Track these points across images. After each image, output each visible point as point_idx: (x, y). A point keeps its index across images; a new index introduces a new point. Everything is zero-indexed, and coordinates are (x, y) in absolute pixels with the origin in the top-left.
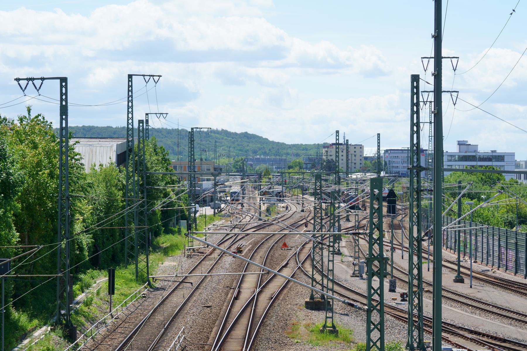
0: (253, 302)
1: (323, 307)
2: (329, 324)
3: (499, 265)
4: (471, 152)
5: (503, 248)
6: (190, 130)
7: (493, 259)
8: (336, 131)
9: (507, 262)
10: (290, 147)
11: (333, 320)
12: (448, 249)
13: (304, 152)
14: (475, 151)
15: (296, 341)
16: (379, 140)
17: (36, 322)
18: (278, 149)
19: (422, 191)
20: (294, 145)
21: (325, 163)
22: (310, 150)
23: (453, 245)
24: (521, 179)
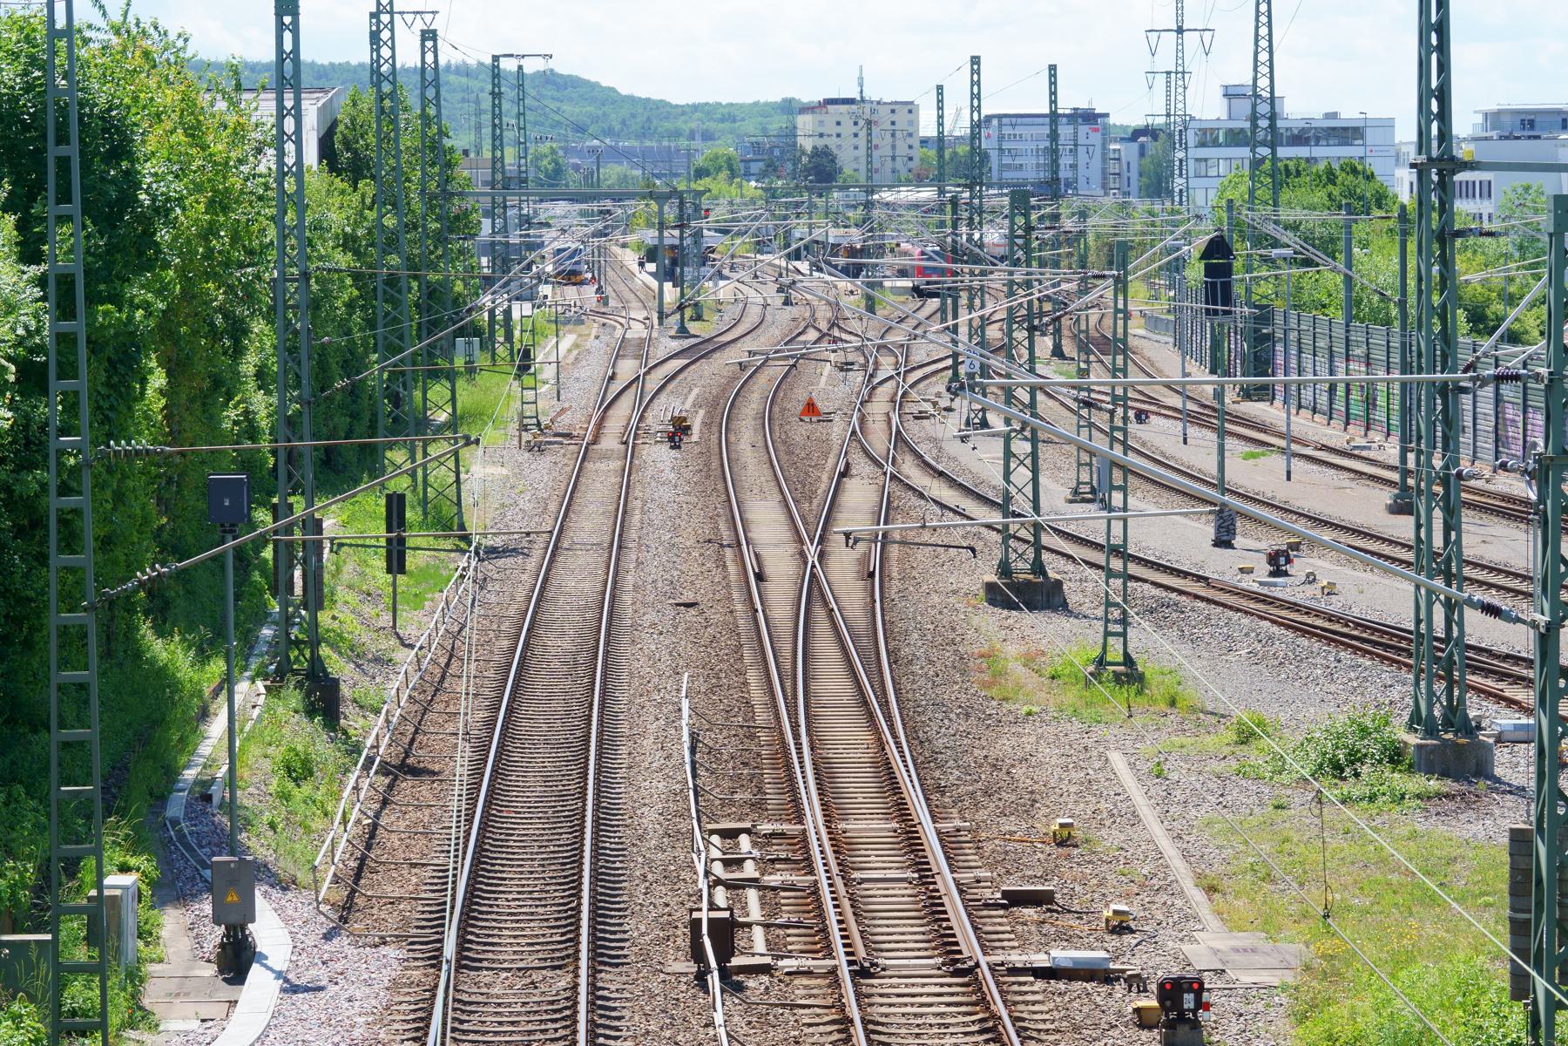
0: (813, 591)
5: (1510, 406)
6: (488, 61)
7: (1475, 441)
8: (972, 57)
10: (684, 113)
12: (1302, 411)
13: (726, 125)
15: (1025, 709)
16: (1055, 83)
17: (217, 667)
18: (649, 120)
19: (1460, 234)
20: (695, 108)
21: (805, 159)
22: (743, 120)
23: (1323, 399)
24: (1490, 196)
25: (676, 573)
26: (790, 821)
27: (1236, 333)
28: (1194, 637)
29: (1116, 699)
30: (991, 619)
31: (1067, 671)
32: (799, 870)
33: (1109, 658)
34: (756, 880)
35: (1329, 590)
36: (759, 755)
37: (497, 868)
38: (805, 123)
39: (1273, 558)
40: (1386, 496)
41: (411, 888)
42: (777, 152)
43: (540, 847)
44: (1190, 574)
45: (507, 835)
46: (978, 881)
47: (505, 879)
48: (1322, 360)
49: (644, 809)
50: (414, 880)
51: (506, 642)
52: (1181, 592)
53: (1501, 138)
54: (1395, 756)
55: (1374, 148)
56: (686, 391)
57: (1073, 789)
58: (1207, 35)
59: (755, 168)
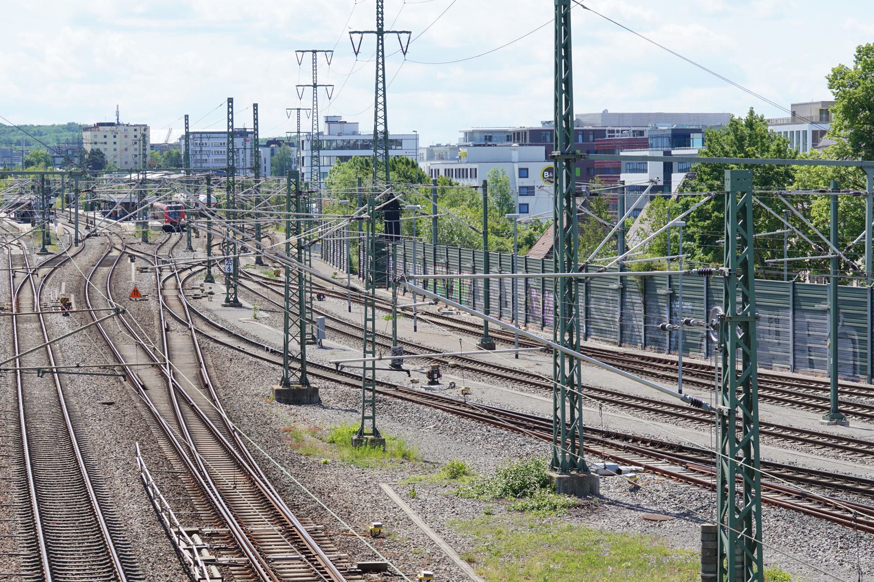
1: (306, 398)
2: (368, 429)
3: (526, 318)
4: (347, 134)
5: (534, 290)
8: (229, 99)
9: (543, 313)
11: (374, 422)
12: (406, 293)
14: (354, 133)
15: (323, 460)
16: (257, 114)
21: (86, 156)
22: (46, 134)
24: (476, 177)
25: (95, 386)
26: (218, 526)
27: (364, 251)
28: (400, 419)
29: (373, 456)
30: (282, 412)
31: (339, 439)
32: (234, 554)
33: (365, 431)
34: (214, 560)
35: (465, 392)
36: (184, 488)
37: (58, 556)
38: (87, 135)
39: (430, 375)
40: (477, 341)
41: (14, 569)
42: (70, 152)
43: (79, 543)
44: (385, 384)
45: (57, 536)
46: (340, 559)
47: (66, 562)
48: (419, 266)
49: (131, 521)
50: (14, 564)
51: (13, 426)
52: (385, 394)
53: (475, 145)
54: (545, 483)
55: (407, 151)
56: (58, 283)
57: (369, 505)
58: (330, 88)
59: (59, 161)
